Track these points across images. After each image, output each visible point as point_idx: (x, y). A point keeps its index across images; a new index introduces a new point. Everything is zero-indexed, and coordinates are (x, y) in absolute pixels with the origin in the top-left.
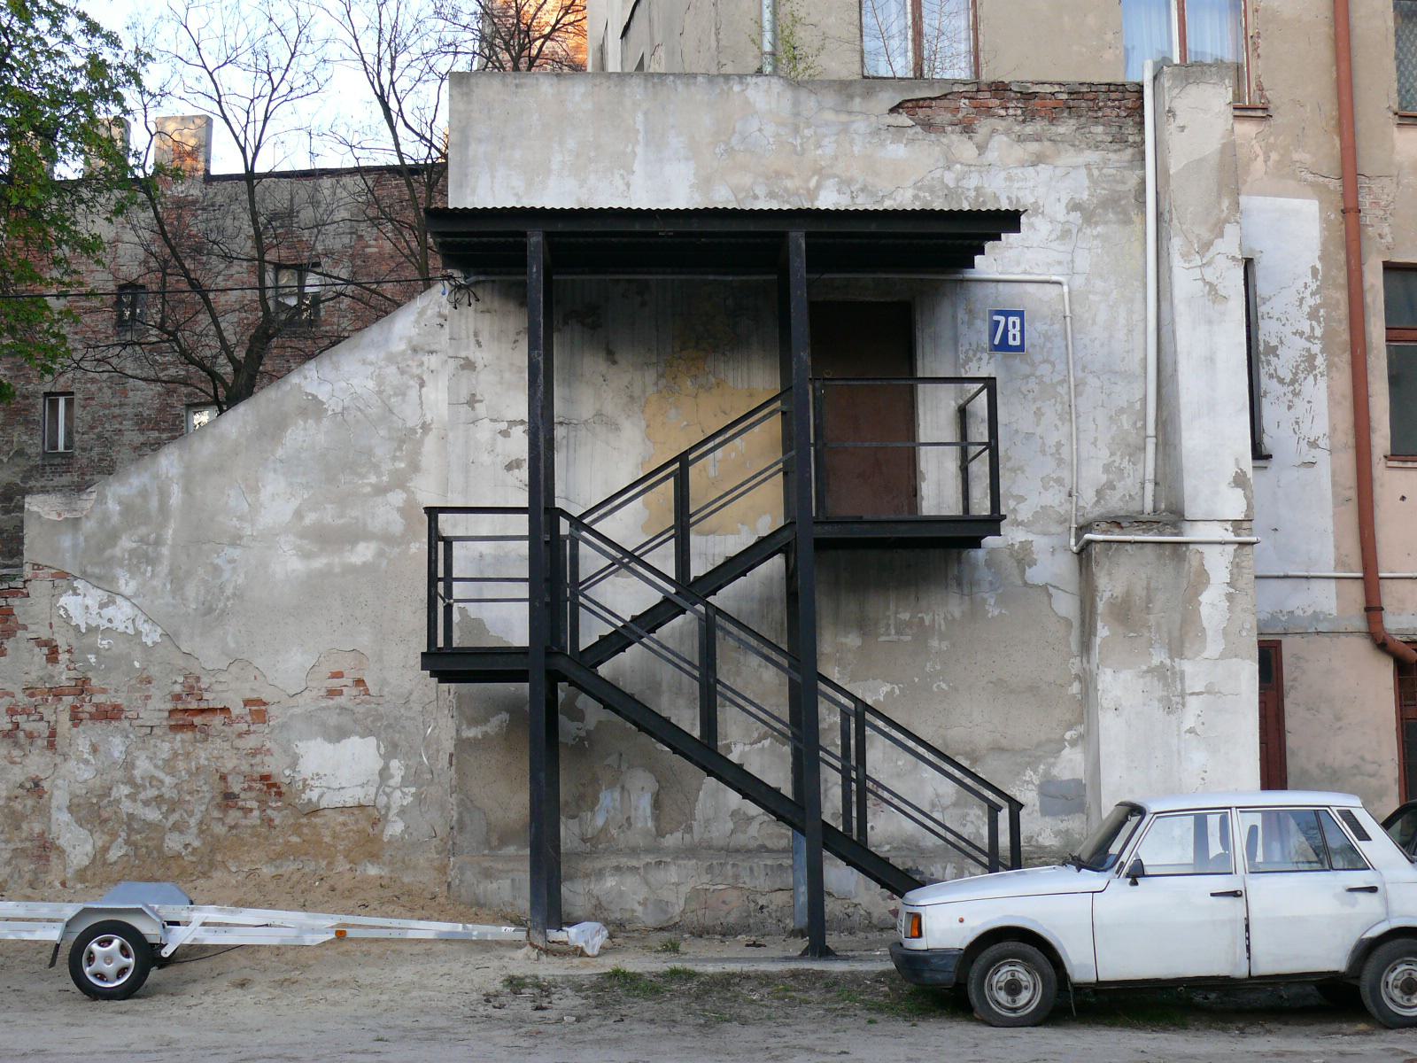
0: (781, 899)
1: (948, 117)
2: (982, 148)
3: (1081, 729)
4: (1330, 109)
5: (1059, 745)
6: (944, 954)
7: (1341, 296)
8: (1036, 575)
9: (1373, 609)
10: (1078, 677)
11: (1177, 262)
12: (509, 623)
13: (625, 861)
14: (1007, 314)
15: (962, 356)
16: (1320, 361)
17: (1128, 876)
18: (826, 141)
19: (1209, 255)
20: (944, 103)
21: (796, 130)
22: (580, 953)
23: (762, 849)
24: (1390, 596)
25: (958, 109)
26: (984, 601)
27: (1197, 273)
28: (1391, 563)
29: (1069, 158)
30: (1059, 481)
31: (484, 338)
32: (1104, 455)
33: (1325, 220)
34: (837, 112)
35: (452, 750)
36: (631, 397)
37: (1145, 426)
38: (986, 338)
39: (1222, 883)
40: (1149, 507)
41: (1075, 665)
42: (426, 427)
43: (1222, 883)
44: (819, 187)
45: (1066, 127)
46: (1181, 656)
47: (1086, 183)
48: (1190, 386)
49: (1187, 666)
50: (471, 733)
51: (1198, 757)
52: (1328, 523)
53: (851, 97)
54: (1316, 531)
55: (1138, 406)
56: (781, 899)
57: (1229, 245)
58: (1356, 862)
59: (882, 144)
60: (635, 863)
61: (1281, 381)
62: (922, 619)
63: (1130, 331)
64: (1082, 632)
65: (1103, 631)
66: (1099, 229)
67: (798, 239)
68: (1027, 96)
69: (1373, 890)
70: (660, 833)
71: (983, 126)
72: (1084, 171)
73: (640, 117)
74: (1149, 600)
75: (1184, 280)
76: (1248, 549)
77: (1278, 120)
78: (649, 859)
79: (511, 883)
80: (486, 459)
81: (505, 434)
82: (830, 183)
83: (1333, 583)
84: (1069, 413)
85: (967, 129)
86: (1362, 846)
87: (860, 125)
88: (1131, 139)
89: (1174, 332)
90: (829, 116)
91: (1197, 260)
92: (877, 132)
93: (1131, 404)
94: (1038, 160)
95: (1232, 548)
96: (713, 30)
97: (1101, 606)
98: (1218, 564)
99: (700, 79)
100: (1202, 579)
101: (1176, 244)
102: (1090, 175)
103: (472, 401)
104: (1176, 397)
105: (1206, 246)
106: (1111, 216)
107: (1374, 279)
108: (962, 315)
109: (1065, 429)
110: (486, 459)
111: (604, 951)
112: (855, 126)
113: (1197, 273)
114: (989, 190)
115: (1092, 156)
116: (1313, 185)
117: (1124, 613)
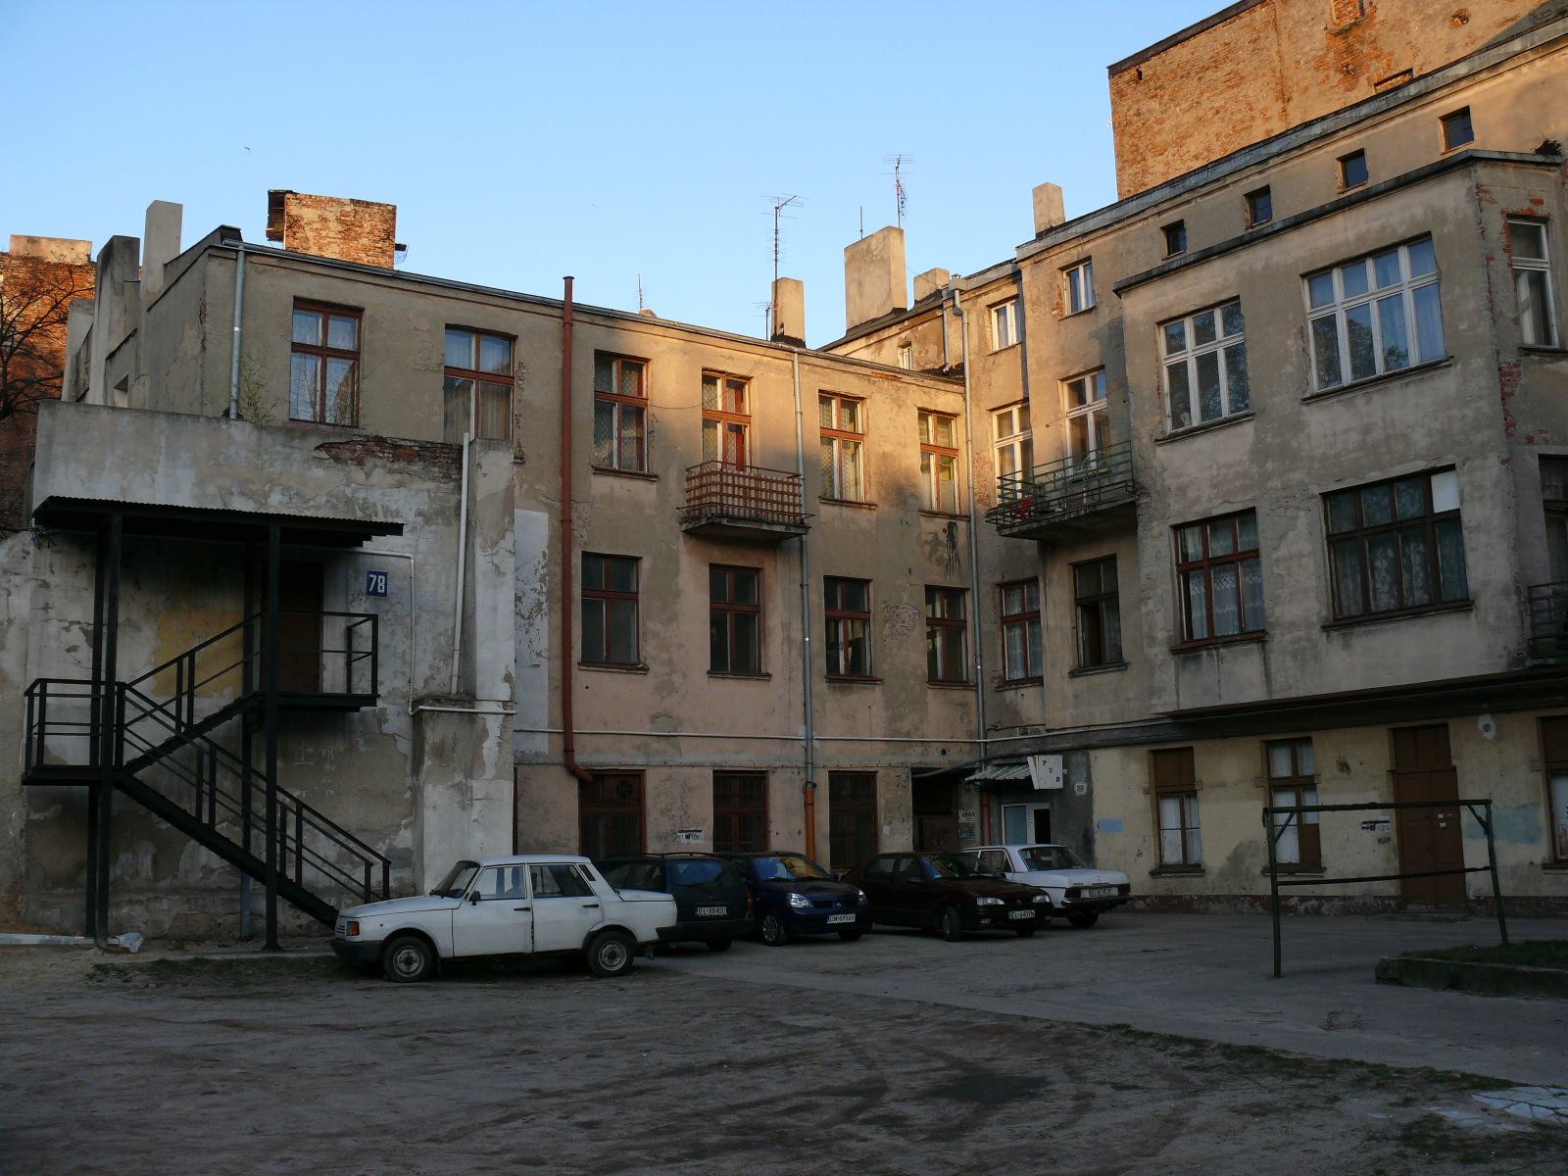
0: (230, 919)
1: (348, 455)
2: (368, 475)
3: (411, 818)
4: (557, 460)
5: (398, 827)
6: (371, 944)
7: (558, 569)
8: (387, 728)
9: (568, 751)
10: (410, 788)
11: (479, 552)
12: (71, 749)
13: (136, 897)
14: (378, 574)
15: (350, 597)
16: (545, 606)
17: (471, 900)
18: (277, 463)
19: (496, 549)
20: (347, 446)
21: (259, 455)
22: (126, 951)
23: (220, 889)
24: (579, 743)
25: (355, 451)
26: (358, 742)
27: (489, 559)
28: (579, 725)
29: (418, 485)
30: (404, 673)
31: (56, 568)
32: (429, 659)
33: (551, 525)
34: (284, 446)
35: (22, 827)
36: (149, 611)
37: (453, 644)
38: (365, 586)
39: (519, 904)
40: (454, 690)
41: (409, 782)
42: (10, 622)
43: (519, 904)
44: (270, 491)
45: (417, 467)
46: (472, 778)
47: (427, 499)
48: (482, 622)
49: (474, 784)
50: (35, 817)
51: (479, 836)
52: (545, 700)
53: (293, 438)
54: (540, 709)
55: (450, 632)
56: (230, 919)
57: (506, 544)
58: (588, 892)
59: (310, 468)
60: (141, 898)
61: (523, 617)
62: (320, 753)
63: (448, 588)
64: (413, 763)
65: (428, 762)
66: (433, 528)
67: (276, 532)
68: (396, 447)
69: (596, 906)
70: (156, 879)
71: (370, 462)
72: (426, 494)
73: (163, 439)
74: (455, 744)
75: (482, 562)
76: (510, 718)
77: (528, 465)
78: (150, 895)
79: (70, 906)
80: (54, 644)
81: (67, 629)
82: (277, 488)
83: (546, 736)
84: (411, 634)
85: (360, 463)
86: (591, 884)
87: (297, 456)
88: (454, 477)
89: (474, 592)
90: (279, 448)
91: (490, 551)
92: (306, 461)
93: (446, 630)
94: (400, 485)
95: (502, 716)
96: (199, 381)
97: (427, 748)
98: (493, 726)
99: (202, 419)
100: (485, 734)
101: (478, 541)
102: (430, 496)
103: (46, 608)
104: (474, 628)
105: (495, 543)
106: (440, 521)
107: (577, 561)
108: (351, 572)
109: (408, 643)
110: (54, 644)
111: (142, 950)
112: (294, 456)
113: (489, 559)
114: (371, 500)
115: (431, 485)
116: (545, 504)
117: (440, 752)
